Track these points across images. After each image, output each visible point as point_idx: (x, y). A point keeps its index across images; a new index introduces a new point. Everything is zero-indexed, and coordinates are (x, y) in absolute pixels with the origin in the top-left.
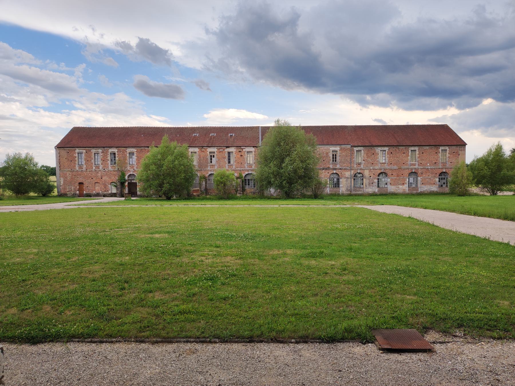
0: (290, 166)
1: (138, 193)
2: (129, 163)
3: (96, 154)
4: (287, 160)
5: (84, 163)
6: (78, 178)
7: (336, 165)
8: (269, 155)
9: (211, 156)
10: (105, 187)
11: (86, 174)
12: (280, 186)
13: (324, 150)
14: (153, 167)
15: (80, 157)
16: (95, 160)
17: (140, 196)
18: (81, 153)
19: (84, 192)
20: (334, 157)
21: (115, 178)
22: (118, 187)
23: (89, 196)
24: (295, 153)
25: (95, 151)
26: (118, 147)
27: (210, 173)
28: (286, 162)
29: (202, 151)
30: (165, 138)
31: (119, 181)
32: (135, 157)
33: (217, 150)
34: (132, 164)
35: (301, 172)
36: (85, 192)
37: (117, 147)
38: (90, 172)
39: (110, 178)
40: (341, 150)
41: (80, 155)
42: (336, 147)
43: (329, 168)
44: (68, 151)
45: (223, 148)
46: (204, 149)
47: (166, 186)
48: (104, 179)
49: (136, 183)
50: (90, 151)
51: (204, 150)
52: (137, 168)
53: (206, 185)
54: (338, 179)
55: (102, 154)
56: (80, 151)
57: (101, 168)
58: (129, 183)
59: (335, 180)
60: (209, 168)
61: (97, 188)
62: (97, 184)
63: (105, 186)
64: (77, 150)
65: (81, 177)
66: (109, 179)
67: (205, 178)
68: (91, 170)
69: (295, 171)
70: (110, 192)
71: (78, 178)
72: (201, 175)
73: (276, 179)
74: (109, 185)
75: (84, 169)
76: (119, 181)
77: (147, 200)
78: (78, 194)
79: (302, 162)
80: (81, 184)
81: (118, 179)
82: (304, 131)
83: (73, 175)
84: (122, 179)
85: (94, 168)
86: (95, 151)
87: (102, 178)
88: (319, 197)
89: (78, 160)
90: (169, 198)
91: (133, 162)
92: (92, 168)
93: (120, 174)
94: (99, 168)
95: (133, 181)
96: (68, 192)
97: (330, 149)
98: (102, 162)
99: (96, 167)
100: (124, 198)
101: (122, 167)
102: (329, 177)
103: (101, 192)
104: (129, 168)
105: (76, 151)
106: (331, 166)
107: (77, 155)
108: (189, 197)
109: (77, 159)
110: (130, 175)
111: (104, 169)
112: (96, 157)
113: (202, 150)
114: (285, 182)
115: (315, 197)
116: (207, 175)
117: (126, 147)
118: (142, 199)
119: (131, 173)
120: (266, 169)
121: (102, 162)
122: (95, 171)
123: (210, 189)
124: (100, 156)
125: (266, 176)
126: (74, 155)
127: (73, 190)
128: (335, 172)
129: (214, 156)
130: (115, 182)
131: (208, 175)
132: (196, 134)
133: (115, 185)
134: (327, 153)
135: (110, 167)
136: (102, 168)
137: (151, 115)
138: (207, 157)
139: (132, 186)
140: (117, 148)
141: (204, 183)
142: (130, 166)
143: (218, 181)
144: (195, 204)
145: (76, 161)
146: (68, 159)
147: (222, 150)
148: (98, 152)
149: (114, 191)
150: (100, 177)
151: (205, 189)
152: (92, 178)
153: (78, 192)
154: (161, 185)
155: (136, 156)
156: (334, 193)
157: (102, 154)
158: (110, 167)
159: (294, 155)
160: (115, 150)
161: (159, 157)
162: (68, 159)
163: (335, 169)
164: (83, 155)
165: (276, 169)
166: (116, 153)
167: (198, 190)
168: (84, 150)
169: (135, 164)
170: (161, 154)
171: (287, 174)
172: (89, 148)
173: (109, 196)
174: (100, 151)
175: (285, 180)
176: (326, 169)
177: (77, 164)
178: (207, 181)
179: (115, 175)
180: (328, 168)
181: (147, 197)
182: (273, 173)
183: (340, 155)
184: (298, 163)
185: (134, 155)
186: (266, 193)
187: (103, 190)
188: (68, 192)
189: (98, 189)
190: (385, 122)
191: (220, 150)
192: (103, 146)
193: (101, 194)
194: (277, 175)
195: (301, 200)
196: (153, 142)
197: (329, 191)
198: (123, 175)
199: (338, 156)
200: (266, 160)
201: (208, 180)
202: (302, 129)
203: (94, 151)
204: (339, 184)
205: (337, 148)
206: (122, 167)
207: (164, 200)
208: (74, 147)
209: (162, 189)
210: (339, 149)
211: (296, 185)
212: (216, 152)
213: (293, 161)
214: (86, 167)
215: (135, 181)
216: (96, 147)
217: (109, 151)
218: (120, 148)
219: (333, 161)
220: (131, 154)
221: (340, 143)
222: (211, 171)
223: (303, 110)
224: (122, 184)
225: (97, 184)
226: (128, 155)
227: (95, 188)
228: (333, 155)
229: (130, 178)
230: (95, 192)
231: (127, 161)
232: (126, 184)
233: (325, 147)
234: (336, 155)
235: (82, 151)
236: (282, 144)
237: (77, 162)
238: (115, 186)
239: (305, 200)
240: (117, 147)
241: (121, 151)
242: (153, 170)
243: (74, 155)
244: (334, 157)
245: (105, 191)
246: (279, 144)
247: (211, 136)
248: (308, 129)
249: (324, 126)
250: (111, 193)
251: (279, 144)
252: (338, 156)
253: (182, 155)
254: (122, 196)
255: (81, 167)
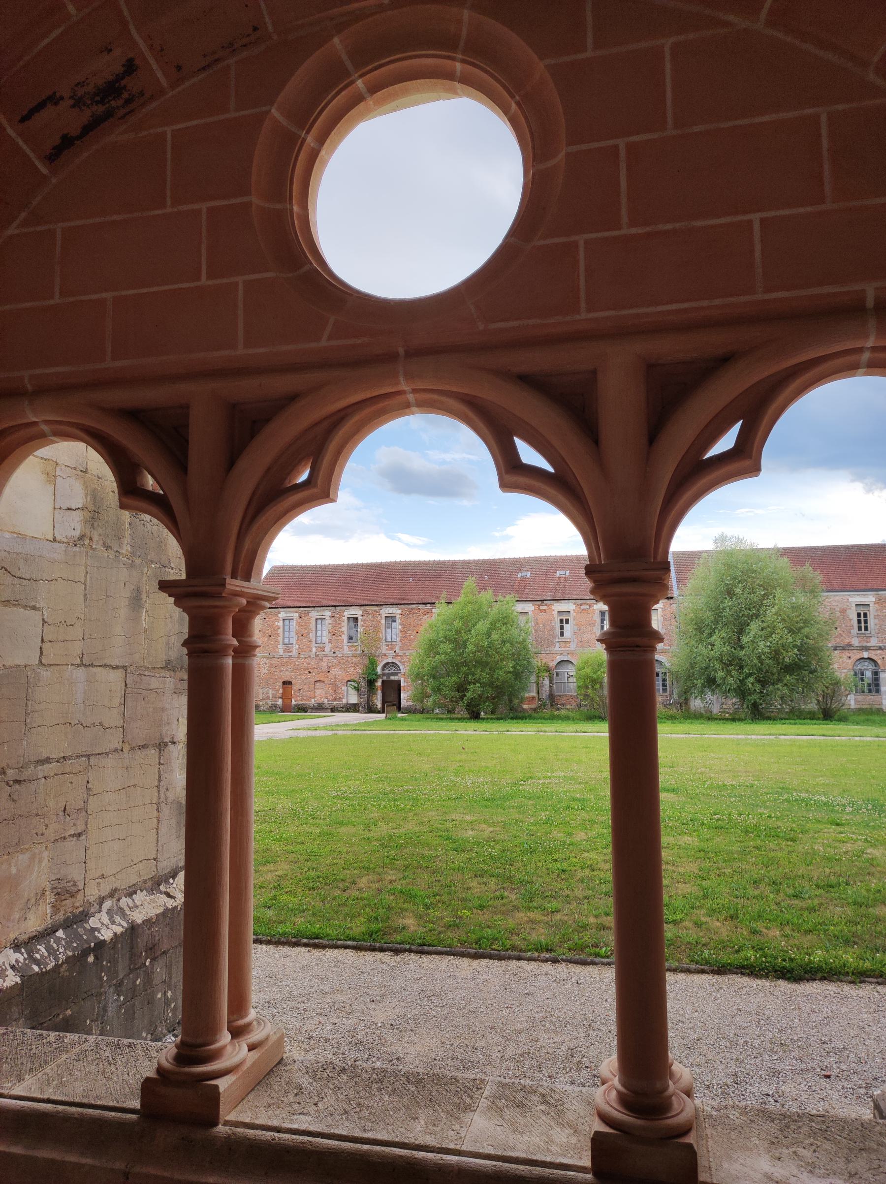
0: (762, 642)
1: (404, 703)
2: (386, 639)
3: (319, 621)
4: (754, 627)
5: (294, 640)
6: (281, 671)
7: (867, 637)
8: (709, 616)
9: (561, 621)
10: (335, 691)
11: (297, 663)
12: (742, 692)
13: (834, 604)
14: (447, 647)
15: (287, 628)
16: (316, 633)
17: (409, 711)
18: (290, 619)
19: (293, 700)
20: (863, 620)
21: (357, 672)
22: (363, 689)
23: (302, 709)
24: (773, 610)
25: (318, 614)
26: (363, 605)
27: (559, 658)
28: (752, 633)
29: (541, 611)
30: (470, 583)
31: (364, 678)
32: (397, 626)
33: (574, 607)
34: (392, 642)
35: (788, 657)
36: (294, 702)
37: (361, 606)
38: (305, 658)
39: (345, 671)
40: (878, 602)
41: (287, 622)
42: (864, 595)
43: (850, 645)
44: (264, 617)
45: (588, 602)
46: (546, 605)
47: (473, 691)
48: (332, 672)
49: (399, 682)
50: (308, 614)
51: (545, 607)
52: (401, 648)
53: (550, 687)
54: (876, 674)
55: (330, 621)
56: (288, 615)
57: (327, 649)
58: (383, 682)
59: (868, 674)
60: (557, 648)
61: (318, 692)
62: (318, 685)
63: (335, 689)
64: (283, 614)
65: (287, 670)
66: (344, 674)
67: (548, 670)
68: (307, 654)
69: (776, 655)
70: (344, 701)
71: (281, 671)
72: (540, 664)
73: (729, 673)
74: (343, 685)
75: (294, 653)
76: (364, 678)
77: (428, 718)
78: (281, 706)
79: (791, 631)
80: (287, 683)
81: (363, 674)
82: (786, 559)
83: (271, 665)
84: (370, 673)
85: (314, 649)
86: (318, 614)
87: (329, 672)
88: (836, 717)
89: (284, 634)
90: (475, 716)
91: (394, 637)
92: (311, 651)
93: (367, 662)
94: (324, 651)
95: (392, 678)
96: (261, 701)
97: (851, 600)
98: (330, 638)
99: (318, 648)
100: (384, 715)
101: (370, 648)
102: (851, 667)
103: (326, 701)
104: (384, 650)
105: (279, 615)
106: (855, 642)
107: (281, 624)
108: (516, 714)
109: (280, 631)
110: (387, 664)
111: (334, 653)
112: (319, 626)
113: (541, 608)
114: (751, 679)
115: (824, 717)
116: (553, 664)
117: (381, 605)
118: (412, 716)
119: (390, 660)
120: (703, 650)
121: (330, 638)
122: (317, 656)
123: (559, 696)
124: (327, 623)
125: (703, 665)
126: (276, 623)
127: (271, 698)
128: (866, 655)
129: (567, 621)
130: (356, 679)
131: (555, 663)
132: (525, 574)
133: (356, 685)
134: (843, 611)
135: (346, 648)
136: (331, 651)
137: (400, 535)
138: (553, 622)
139: (392, 690)
140: (363, 608)
141: (547, 682)
142: (387, 646)
143: (587, 676)
144: (585, 729)
145: (278, 635)
146: (264, 633)
147: (587, 607)
148: (323, 617)
149: (353, 699)
150: (325, 669)
151: (549, 694)
152: (310, 672)
153: (280, 702)
154: (461, 688)
155: (400, 624)
156: (868, 707)
157: (330, 621)
158: (346, 648)
159: (770, 614)
160: (357, 612)
161: (458, 624)
162: (264, 633)
163: (867, 649)
164: (294, 623)
165: (726, 648)
166: (360, 618)
167: (533, 698)
168: (296, 612)
169: (398, 640)
170: (462, 618)
171: (756, 661)
172: (305, 609)
173: (344, 709)
174: (327, 613)
175: (750, 675)
176: (843, 649)
177: (281, 642)
178: (553, 678)
179: (355, 665)
180: (848, 647)
181: (420, 711)
182: (720, 660)
183: (878, 615)
184: (782, 636)
185: (395, 621)
186: (696, 704)
187: (331, 698)
188: (261, 701)
189: (321, 695)
190: (304, 531)
191: (582, 607)
192: (333, 604)
193: (327, 705)
194: (733, 663)
195: (795, 724)
196: (444, 594)
197: (852, 702)
198: (373, 664)
199: (872, 617)
200: (700, 630)
201: (555, 676)
202: (781, 555)
203: (314, 614)
204: (877, 685)
205: (869, 598)
206: (370, 648)
207: (460, 719)
208: (278, 608)
209: (465, 696)
210: (874, 600)
211: (779, 686)
212: (572, 612)
213: (768, 632)
214: (299, 648)
215: (396, 678)
216: (320, 607)
217: (345, 614)
218: (367, 608)
219: (860, 628)
220: (391, 619)
221: (875, 587)
222: (561, 654)
223: (747, 510)
224: (371, 683)
225: (318, 684)
226: (383, 622)
227: (315, 692)
228: (859, 615)
229: (387, 671)
230: (315, 701)
231: (382, 635)
232: (379, 683)
233: (837, 595)
234: (865, 615)
235: (291, 615)
236: (738, 590)
237: (280, 639)
238: (355, 687)
239: (805, 724)
240: (361, 606)
241: (370, 614)
242: (446, 653)
243: (276, 623)
244: (863, 620)
245: (335, 699)
246: (730, 593)
247: (559, 578)
248: (798, 555)
249: (828, 547)
250: (347, 704)
251: (730, 593)
252: (872, 617)
253: (506, 620)
254: (371, 709)
255: (288, 646)
